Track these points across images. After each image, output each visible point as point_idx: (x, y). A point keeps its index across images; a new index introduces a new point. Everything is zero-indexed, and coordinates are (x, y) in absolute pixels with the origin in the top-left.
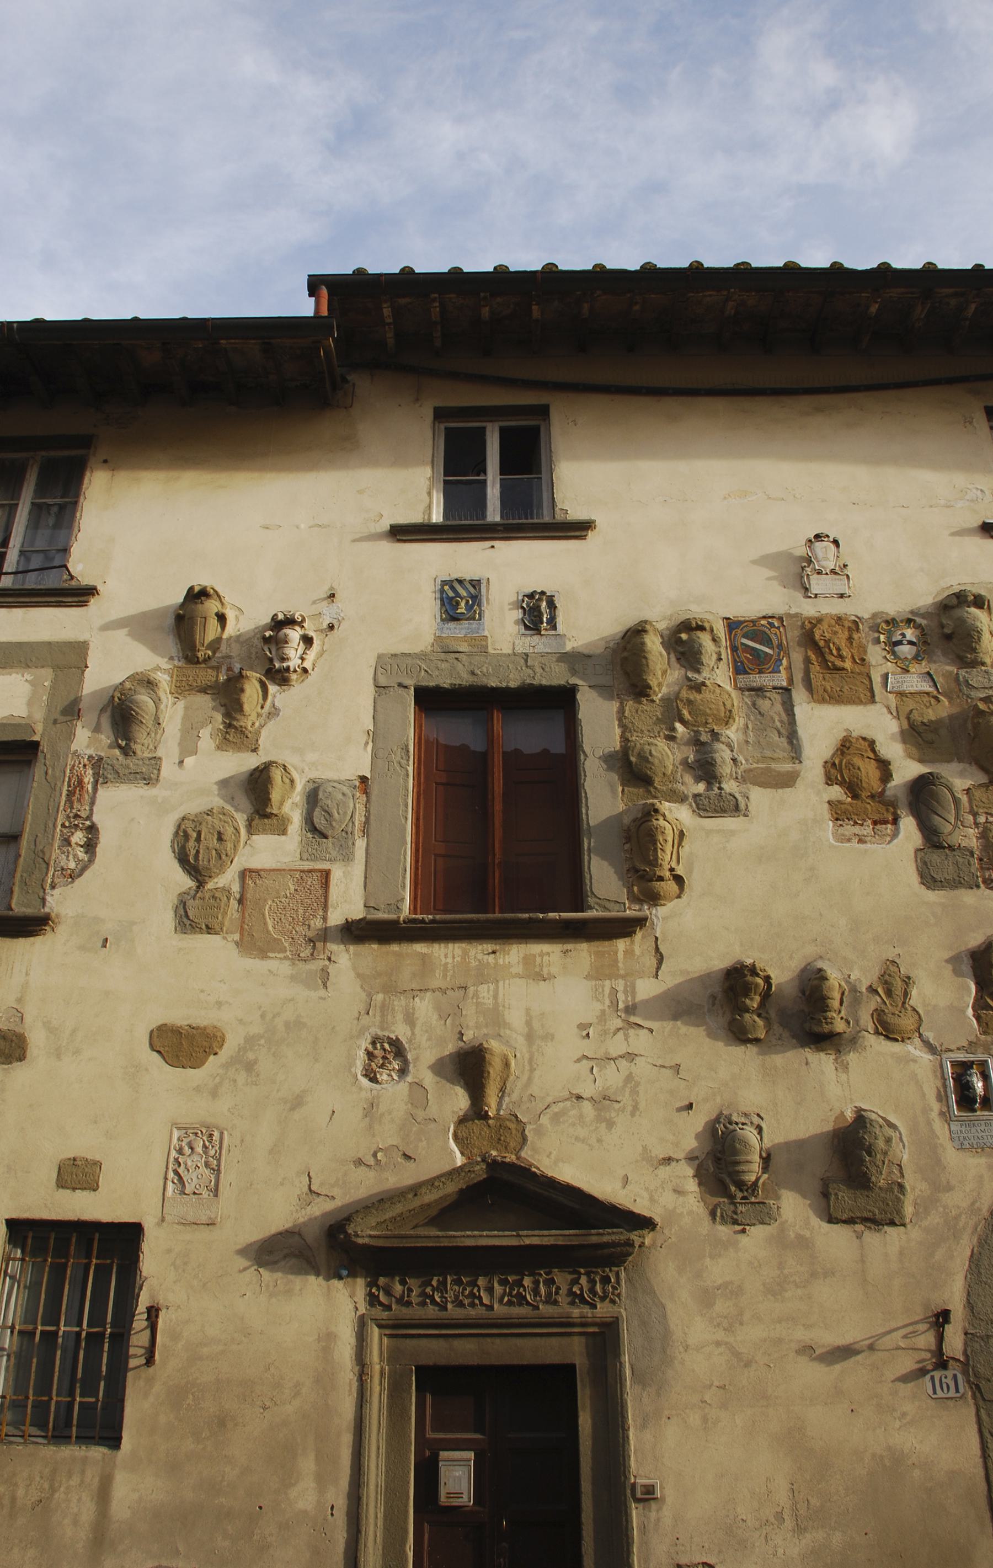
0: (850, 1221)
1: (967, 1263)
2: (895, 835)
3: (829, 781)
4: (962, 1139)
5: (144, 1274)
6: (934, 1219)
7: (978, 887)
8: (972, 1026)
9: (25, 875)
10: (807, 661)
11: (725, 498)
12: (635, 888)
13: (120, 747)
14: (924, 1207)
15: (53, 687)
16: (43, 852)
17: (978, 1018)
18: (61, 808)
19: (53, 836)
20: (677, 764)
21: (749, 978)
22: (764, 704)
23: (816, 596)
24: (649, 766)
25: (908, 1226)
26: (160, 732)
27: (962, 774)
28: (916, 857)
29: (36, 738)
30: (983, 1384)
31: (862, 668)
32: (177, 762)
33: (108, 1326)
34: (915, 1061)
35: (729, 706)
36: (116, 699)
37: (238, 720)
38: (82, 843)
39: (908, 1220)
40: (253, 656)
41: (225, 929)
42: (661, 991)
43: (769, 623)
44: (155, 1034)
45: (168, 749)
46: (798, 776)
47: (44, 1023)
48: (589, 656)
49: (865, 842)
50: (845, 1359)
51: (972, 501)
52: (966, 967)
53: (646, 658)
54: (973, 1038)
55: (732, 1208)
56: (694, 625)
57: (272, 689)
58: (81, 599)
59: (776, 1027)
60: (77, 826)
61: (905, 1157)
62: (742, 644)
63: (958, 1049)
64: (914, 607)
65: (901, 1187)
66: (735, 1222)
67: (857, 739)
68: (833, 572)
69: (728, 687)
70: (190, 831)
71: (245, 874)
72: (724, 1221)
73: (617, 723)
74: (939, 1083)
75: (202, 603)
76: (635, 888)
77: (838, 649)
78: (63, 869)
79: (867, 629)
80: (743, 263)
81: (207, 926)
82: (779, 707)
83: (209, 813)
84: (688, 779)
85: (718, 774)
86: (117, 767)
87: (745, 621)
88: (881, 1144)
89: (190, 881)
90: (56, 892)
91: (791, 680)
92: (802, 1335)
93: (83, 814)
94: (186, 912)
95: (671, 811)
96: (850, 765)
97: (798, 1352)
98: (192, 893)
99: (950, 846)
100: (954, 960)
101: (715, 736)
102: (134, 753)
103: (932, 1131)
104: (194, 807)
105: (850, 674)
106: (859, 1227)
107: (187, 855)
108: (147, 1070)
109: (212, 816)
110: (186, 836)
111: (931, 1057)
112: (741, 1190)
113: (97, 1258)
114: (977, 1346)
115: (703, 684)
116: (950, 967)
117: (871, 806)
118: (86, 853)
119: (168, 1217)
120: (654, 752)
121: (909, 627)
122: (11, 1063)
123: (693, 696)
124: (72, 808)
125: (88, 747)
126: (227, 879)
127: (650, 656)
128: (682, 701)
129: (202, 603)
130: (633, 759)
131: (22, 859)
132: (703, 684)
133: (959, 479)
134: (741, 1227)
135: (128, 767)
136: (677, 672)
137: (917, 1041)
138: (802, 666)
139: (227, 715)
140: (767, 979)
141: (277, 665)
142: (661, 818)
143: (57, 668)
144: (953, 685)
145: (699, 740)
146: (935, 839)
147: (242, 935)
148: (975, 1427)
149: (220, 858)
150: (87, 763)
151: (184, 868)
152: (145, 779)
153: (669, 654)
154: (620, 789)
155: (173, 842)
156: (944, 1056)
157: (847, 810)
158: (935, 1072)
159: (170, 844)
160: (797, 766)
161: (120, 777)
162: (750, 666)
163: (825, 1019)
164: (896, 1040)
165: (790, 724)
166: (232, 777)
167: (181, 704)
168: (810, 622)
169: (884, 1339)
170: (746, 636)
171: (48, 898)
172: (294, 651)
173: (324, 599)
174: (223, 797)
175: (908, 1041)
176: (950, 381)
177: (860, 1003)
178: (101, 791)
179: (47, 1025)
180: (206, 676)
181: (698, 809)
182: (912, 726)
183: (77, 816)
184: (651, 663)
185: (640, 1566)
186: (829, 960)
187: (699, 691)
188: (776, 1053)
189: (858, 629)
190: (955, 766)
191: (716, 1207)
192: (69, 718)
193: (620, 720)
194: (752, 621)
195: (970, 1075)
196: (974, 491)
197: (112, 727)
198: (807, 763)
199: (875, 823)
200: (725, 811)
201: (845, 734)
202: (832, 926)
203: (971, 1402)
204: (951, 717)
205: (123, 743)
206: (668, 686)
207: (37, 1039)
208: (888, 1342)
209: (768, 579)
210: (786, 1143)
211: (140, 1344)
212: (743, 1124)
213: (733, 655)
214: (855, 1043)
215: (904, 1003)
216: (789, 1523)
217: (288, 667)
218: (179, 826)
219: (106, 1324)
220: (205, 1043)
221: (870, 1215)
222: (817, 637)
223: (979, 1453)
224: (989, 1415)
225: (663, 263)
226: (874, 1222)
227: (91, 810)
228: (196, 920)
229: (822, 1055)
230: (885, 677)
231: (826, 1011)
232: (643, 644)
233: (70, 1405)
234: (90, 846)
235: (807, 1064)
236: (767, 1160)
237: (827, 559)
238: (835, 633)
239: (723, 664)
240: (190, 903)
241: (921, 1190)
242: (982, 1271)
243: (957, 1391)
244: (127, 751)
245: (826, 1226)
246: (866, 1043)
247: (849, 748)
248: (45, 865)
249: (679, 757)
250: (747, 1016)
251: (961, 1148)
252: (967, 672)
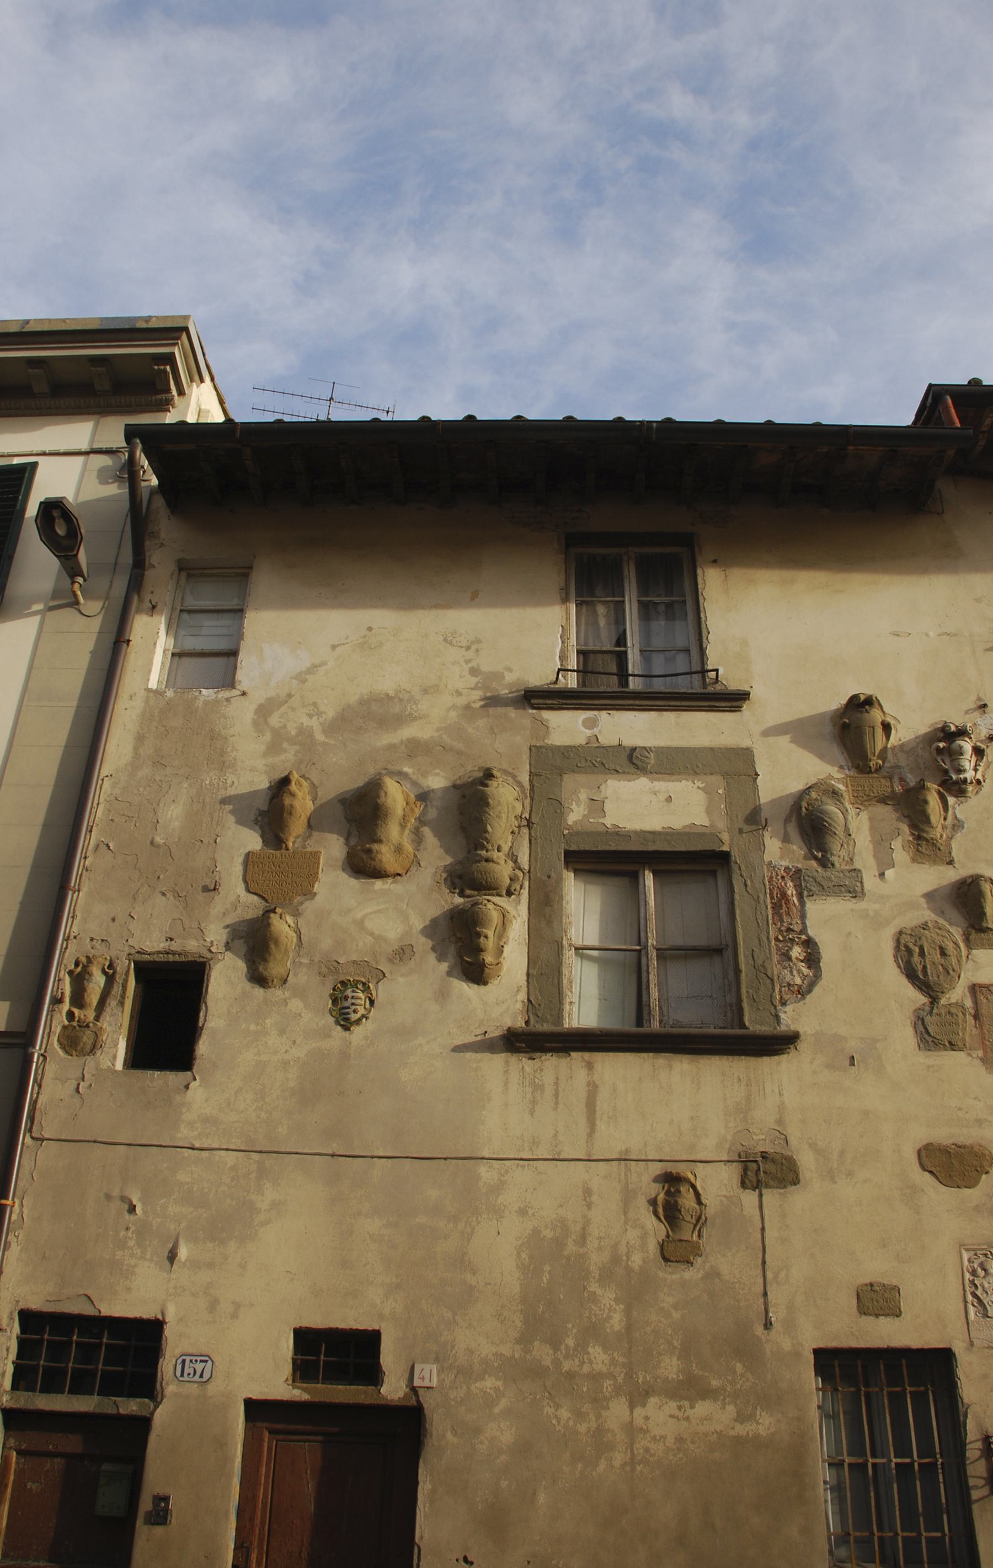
5: (966, 1401)
9: (751, 991)
13: (816, 858)
15: (728, 796)
16: (764, 967)
18: (770, 921)
19: (770, 950)
26: (851, 843)
29: (725, 848)
32: (877, 874)
33: (938, 1456)
36: (804, 809)
37: (927, 832)
38: (802, 958)
40: (922, 766)
41: (967, 1045)
44: (923, 1153)
45: (865, 860)
47: (810, 1145)
57: (951, 800)
58: (735, 704)
60: (792, 940)
70: (911, 945)
71: (974, 989)
75: (867, 712)
78: (789, 985)
81: (950, 1043)
83: (925, 926)
86: (819, 879)
89: (923, 997)
90: (789, 1008)
93: (797, 928)
94: (926, 1029)
98: (927, 1009)
102: (833, 865)
104: (910, 920)
107: (914, 971)
108: (923, 1191)
109: (929, 930)
110: (909, 951)
113: (910, 1386)
118: (809, 968)
119: (976, 1342)
122: (785, 1187)
124: (782, 921)
125: (782, 858)
126: (957, 994)
129: (867, 712)
131: (743, 975)
135: (830, 879)
139: (913, 826)
141: (954, 777)
143: (726, 775)
147: (985, 1051)
149: (948, 973)
150: (785, 875)
151: (913, 984)
152: (850, 892)
155: (895, 956)
159: (893, 959)
161: (827, 890)
166: (935, 890)
167: (864, 816)
171: (782, 1016)
172: (968, 761)
173: (975, 710)
174: (933, 911)
178: (809, 905)
179: (813, 1146)
180: (881, 786)
183: (789, 930)
185: (259, 1563)
192: (754, 827)
197: (802, 837)
205: (820, 855)
207: (806, 1161)
211: (978, 1474)
217: (966, 779)
218: (898, 941)
219: (935, 1454)
220: (975, 1162)
227: (804, 924)
228: (938, 1037)
233: (917, 1541)
234: (813, 959)
240: (928, 1019)
244: (825, 863)
248: (768, 981)
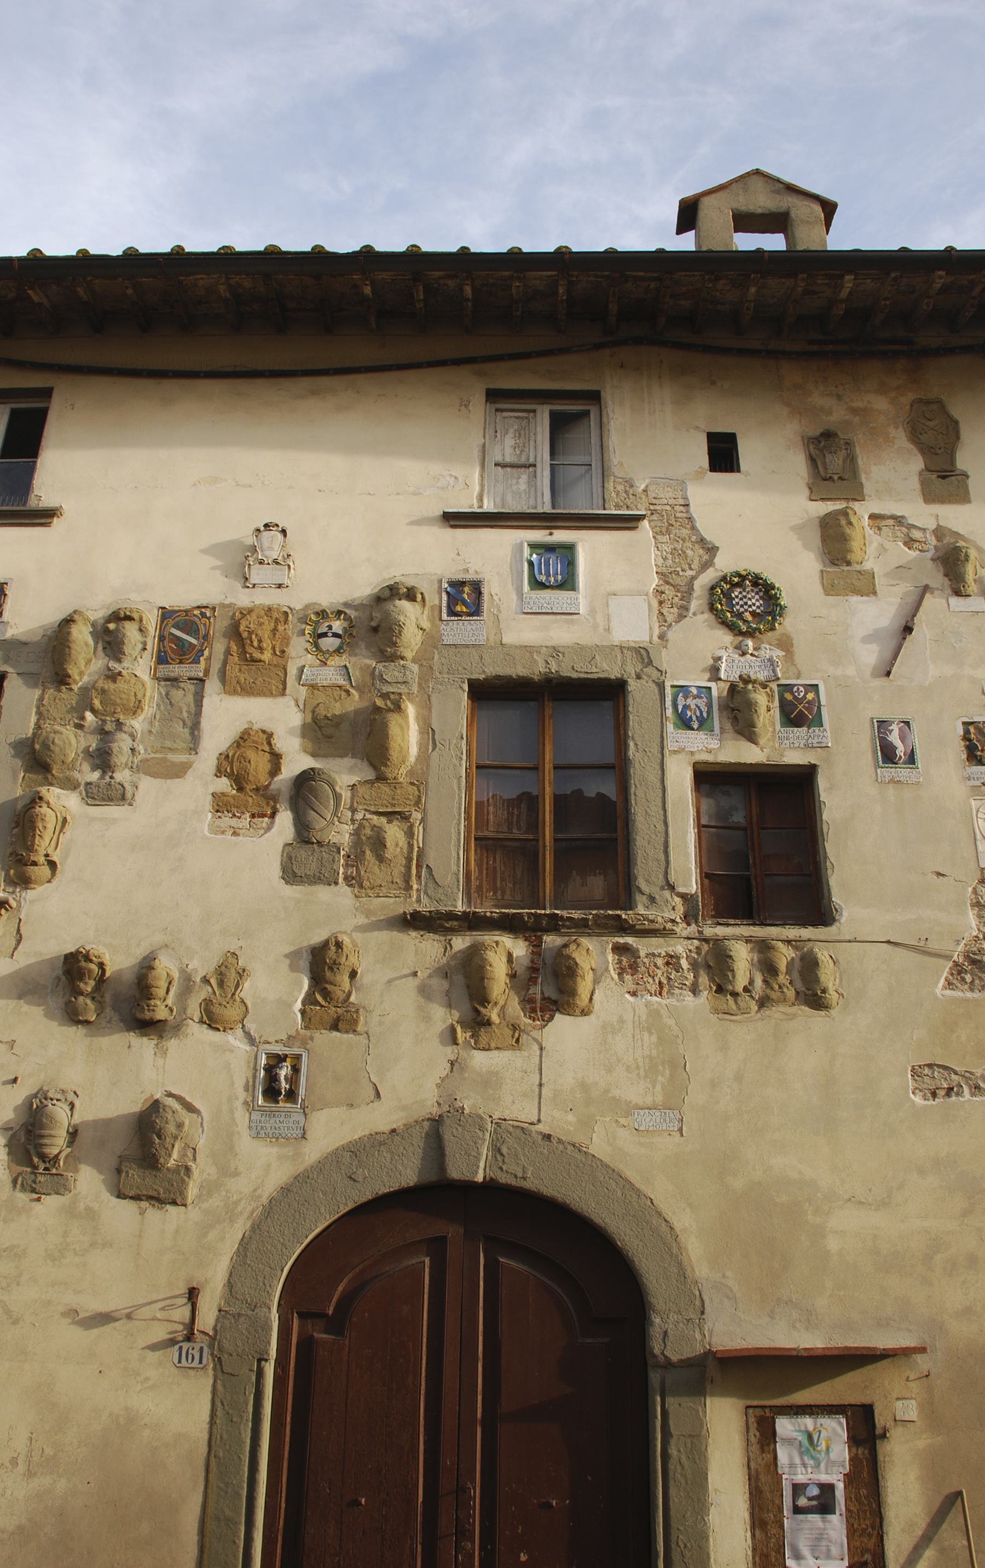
0: (136, 1198)
1: (237, 1245)
2: (269, 828)
3: (219, 772)
4: (259, 1128)
6: (215, 1202)
7: (336, 883)
8: (295, 1021)
10: (228, 652)
11: (194, 485)
12: (12, 872)
14: (209, 1189)
17: (303, 1012)
20: (79, 752)
21: (83, 964)
22: (177, 695)
23: (254, 585)
24: (49, 753)
25: (189, 1207)
27: (351, 770)
28: (283, 852)
30: (225, 1357)
31: (280, 661)
34: (232, 1051)
35: (140, 696)
39: (189, 1201)
42: (13, 970)
43: (202, 614)
46: (191, 766)
48: (26, 644)
49: (239, 835)
50: (103, 1325)
51: (443, 488)
52: (304, 963)
53: (69, 647)
54: (293, 1033)
55: (33, 1177)
56: (122, 615)
59: (108, 1011)
61: (202, 1141)
63: (277, 1042)
64: (350, 598)
65: (188, 1170)
66: (34, 1191)
67: (257, 732)
68: (276, 562)
69: (145, 677)
72: (23, 1189)
73: (35, 710)
74: (250, 1074)
76: (12, 872)
77: (260, 641)
79: (296, 621)
80: (224, 247)
82: (190, 698)
84: (86, 767)
85: (112, 763)
88: (171, 1128)
91: (207, 672)
92: (70, 1299)
95: (59, 797)
96: (243, 758)
97: (64, 1315)
99: (318, 842)
100: (293, 956)
101: (119, 725)
103: (233, 1119)
105: (267, 666)
106: (144, 1204)
111: (248, 1048)
112: (44, 1162)
114: (227, 1323)
115: (120, 674)
116: (288, 962)
117: (252, 800)
120: (56, 741)
121: (339, 619)
123: (110, 686)
127: (73, 646)
128: (97, 690)
130: (37, 747)
132: (120, 674)
133: (436, 468)
134: (36, 1196)
136: (101, 662)
137: (239, 1032)
138: (222, 657)
140: (101, 965)
142: (45, 806)
144: (368, 679)
145: (103, 729)
146: (306, 834)
148: (209, 1396)
153: (96, 643)
154: (22, 774)
156: (262, 1047)
157: (228, 802)
158: (249, 1062)
160: (192, 757)
163: (148, 1006)
164: (218, 1030)
165: (196, 715)
168: (241, 613)
169: (144, 1309)
175: (230, 1032)
176: (458, 362)
177: (191, 992)
181: (87, 797)
182: (315, 720)
184: (73, 652)
186: (173, 949)
187: (115, 681)
188: (104, 1036)
189: (286, 621)
190: (348, 761)
191: (19, 1174)
193: (38, 708)
194: (186, 611)
195: (281, 1068)
196: (448, 478)
198: (203, 753)
199: (253, 816)
200: (111, 800)
201: (246, 726)
202: (186, 916)
203: (211, 1372)
204: (357, 712)
206: (90, 675)
208: (146, 1312)
209: (213, 568)
210: (94, 1121)
212: (58, 1100)
213: (159, 644)
214: (179, 1030)
215: (234, 994)
216: (22, 1468)
221: (155, 1194)
222: (242, 628)
223: (208, 1419)
224: (224, 1386)
225: (145, 248)
226: (158, 1200)
229: (145, 1039)
230: (301, 670)
231: (150, 999)
232: (69, 633)
235: (129, 1047)
236: (73, 1134)
237: (271, 549)
238: (261, 624)
239: (147, 654)
241: (209, 1174)
242: (248, 1254)
243: (201, 1362)
245: (115, 1201)
246: (189, 1031)
247: (245, 741)
249: (83, 744)
250: (81, 999)
251: (257, 1136)
252: (384, 666)
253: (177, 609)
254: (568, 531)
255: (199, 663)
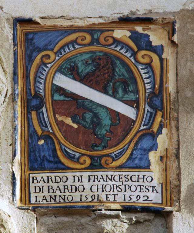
43: (135, 36)
62: (60, 90)
87: (73, 30)
162: (71, 148)
170: (73, 72)
194: (91, 30)
213: (27, 117)
253: (66, 23)
254: (20, 186)
255: (148, 167)
